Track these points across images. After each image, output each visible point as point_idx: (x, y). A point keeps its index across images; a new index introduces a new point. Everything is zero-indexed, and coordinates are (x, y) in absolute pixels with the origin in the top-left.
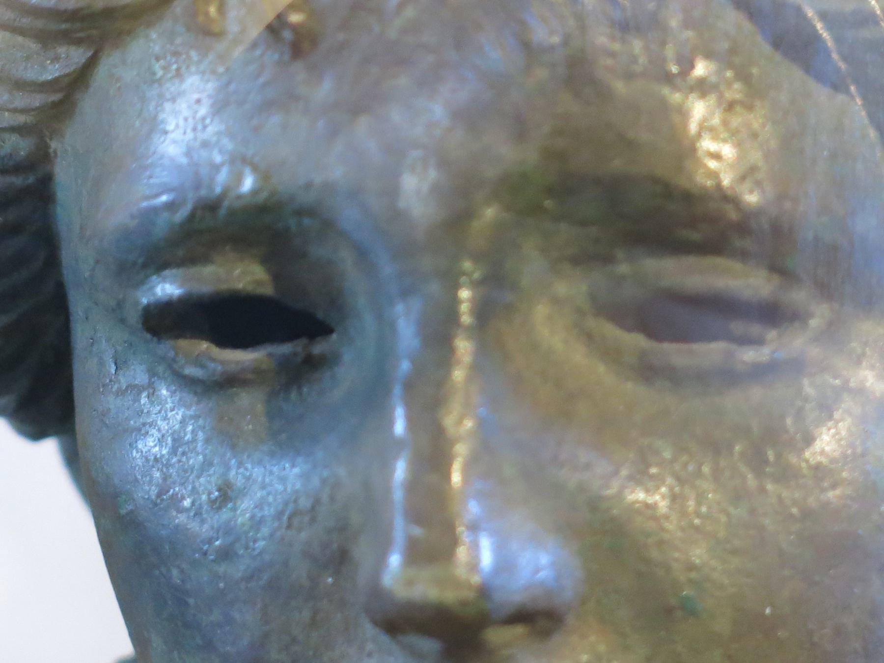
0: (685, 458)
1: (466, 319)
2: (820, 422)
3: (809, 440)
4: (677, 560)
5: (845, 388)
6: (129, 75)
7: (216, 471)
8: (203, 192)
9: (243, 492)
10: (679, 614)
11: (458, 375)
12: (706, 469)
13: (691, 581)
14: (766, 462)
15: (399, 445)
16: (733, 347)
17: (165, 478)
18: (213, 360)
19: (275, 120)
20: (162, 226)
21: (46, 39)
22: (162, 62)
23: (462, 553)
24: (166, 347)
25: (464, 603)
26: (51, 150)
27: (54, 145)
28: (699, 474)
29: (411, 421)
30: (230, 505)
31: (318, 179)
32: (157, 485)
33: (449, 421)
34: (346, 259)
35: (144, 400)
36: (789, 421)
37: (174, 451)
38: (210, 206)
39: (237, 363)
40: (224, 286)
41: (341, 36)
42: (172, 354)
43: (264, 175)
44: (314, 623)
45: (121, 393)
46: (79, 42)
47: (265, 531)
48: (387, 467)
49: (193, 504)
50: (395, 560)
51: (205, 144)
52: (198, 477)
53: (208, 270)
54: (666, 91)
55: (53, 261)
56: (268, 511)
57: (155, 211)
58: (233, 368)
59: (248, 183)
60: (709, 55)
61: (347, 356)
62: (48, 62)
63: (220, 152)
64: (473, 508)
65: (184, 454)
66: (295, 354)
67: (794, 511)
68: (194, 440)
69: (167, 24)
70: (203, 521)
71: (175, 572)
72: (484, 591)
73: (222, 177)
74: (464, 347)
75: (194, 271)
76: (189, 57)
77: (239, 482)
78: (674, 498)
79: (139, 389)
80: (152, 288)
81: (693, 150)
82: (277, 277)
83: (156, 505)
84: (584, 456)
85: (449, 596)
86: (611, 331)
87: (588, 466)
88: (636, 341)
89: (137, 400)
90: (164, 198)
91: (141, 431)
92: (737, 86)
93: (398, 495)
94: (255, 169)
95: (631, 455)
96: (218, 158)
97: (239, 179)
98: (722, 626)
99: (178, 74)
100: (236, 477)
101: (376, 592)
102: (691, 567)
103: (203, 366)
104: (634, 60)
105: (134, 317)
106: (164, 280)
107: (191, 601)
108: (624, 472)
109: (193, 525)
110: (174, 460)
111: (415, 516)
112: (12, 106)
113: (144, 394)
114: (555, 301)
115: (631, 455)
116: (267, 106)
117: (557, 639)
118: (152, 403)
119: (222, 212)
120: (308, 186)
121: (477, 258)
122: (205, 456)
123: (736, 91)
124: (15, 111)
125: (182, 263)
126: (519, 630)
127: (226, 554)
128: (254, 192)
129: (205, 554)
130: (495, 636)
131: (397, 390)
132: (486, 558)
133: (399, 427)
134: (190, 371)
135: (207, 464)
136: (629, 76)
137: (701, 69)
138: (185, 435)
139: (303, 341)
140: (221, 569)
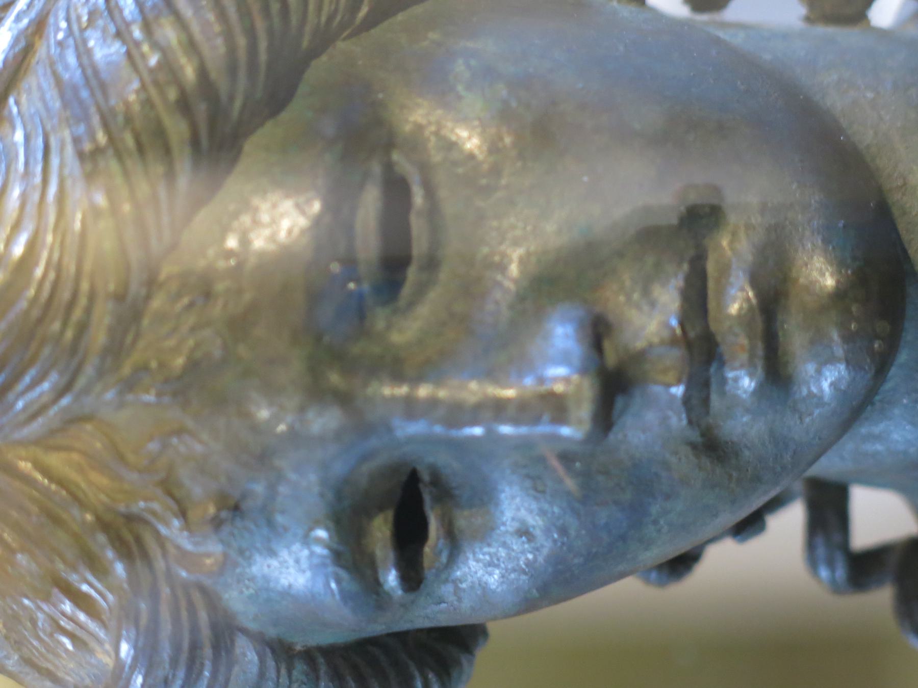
2: (461, 151)
3: (471, 156)
5: (437, 133)
7: (509, 540)
8: (328, 561)
9: (523, 522)
11: (442, 394)
12: (495, 223)
15: (490, 432)
17: (514, 570)
18: (436, 545)
19: (280, 519)
20: (352, 586)
22: (244, 589)
23: (559, 388)
24: (429, 574)
26: (302, 649)
27: (298, 648)
29: (474, 423)
30: (531, 530)
32: (519, 576)
34: (367, 468)
35: (464, 586)
37: (497, 566)
38: (337, 557)
39: (438, 530)
42: (434, 571)
43: (317, 524)
45: (460, 600)
47: (546, 506)
49: (530, 552)
50: (566, 431)
51: (297, 561)
52: (513, 550)
55: (373, 641)
57: (341, 591)
59: (322, 533)
60: (223, 239)
61: (430, 459)
62: (246, 659)
63: (301, 551)
64: (529, 381)
65: (498, 560)
68: (489, 554)
70: (542, 546)
71: (576, 561)
73: (319, 550)
75: (379, 562)
77: (516, 525)
78: (516, 243)
79: (457, 588)
80: (392, 589)
82: (381, 509)
83: (532, 576)
84: (490, 307)
86: (407, 291)
87: (497, 303)
88: (412, 274)
89: (464, 590)
90: (333, 585)
91: (484, 587)
93: (523, 430)
94: (311, 529)
96: (306, 552)
97: (318, 541)
100: (511, 526)
103: (440, 552)
105: (411, 596)
106: (386, 581)
107: (594, 550)
109: (545, 551)
110: (502, 565)
112: (276, 679)
113: (460, 585)
114: (389, 327)
116: (270, 523)
118: (466, 581)
119: (341, 548)
120: (322, 495)
122: (499, 546)
123: (246, 219)
124: (278, 677)
126: (607, 345)
127: (563, 531)
128: (327, 529)
129: (563, 544)
130: (611, 359)
131: (455, 433)
132: (560, 371)
133: (478, 431)
134: (444, 558)
135: (504, 545)
138: (485, 559)
139: (421, 486)
140: (572, 533)
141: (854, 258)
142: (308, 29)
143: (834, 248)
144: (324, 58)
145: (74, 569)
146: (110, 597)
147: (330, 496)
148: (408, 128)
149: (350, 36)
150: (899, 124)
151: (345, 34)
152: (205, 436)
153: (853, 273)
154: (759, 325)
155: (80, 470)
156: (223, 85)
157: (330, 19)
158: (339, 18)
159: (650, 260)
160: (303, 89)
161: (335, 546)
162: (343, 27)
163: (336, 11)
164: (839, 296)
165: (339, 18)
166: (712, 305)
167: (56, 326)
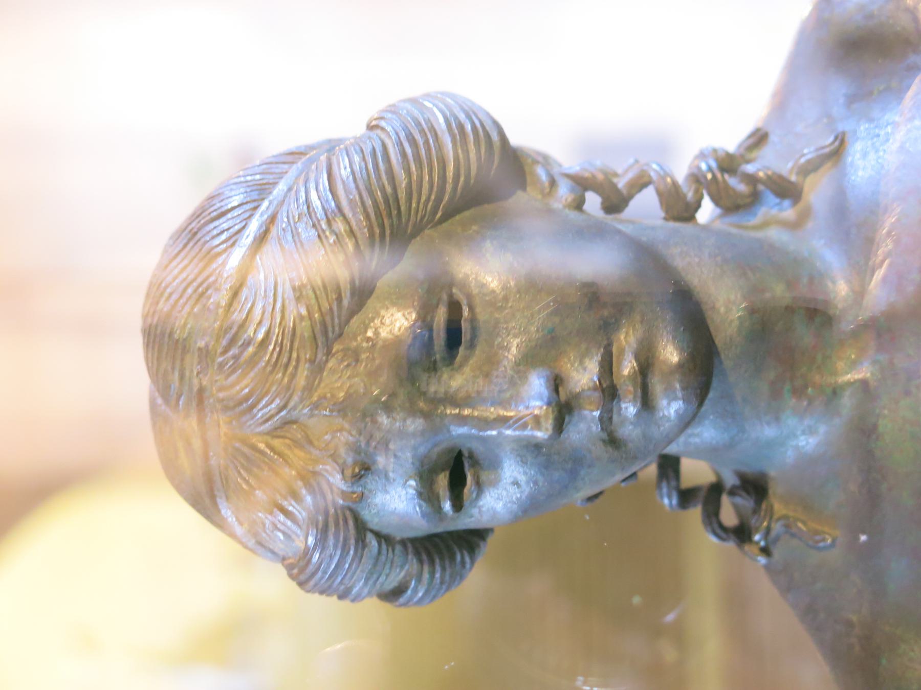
0: (501, 333)
1: (457, 411)
4: (536, 336)
6: (376, 520)
9: (515, 478)
10: (553, 334)
13: (542, 331)
14: (502, 306)
15: (500, 434)
16: (463, 319)
21: (364, 546)
24: (466, 503)
25: (553, 412)
28: (506, 328)
29: (492, 429)
31: (410, 460)
33: (492, 417)
36: (487, 298)
40: (447, 488)
41: (363, 454)
43: (410, 477)
44: (559, 454)
45: (481, 516)
46: (365, 536)
48: (507, 436)
53: (441, 493)
54: (378, 346)
56: (521, 470)
57: (422, 512)
58: (473, 482)
61: (469, 445)
66: (468, 462)
67: (518, 296)
69: (359, 509)
72: (549, 404)
74: (466, 412)
76: (370, 502)
78: (515, 336)
80: (448, 511)
81: (397, 337)
82: (443, 470)
85: (551, 416)
88: (462, 350)
92: (376, 321)
94: (407, 481)
95: (501, 352)
97: (410, 486)
98: (557, 320)
99: (376, 505)
100: (510, 480)
101: (550, 438)
102: (538, 330)
103: (473, 493)
104: (367, 357)
105: (457, 515)
108: (506, 354)
111: (524, 426)
115: (501, 352)
117: (563, 375)
120: (413, 463)
121: (436, 409)
125: (439, 502)
126: (560, 389)
127: (536, 483)
130: (563, 397)
133: (494, 433)
134: (474, 495)
136: (374, 359)
137: (370, 334)
140: (541, 484)
145: (286, 499)
150: (712, 275)
151: (429, 226)
154: (639, 379)
157: (423, 217)
158: (426, 218)
162: (429, 222)
164: (680, 365)
165: (426, 218)
166: (614, 369)
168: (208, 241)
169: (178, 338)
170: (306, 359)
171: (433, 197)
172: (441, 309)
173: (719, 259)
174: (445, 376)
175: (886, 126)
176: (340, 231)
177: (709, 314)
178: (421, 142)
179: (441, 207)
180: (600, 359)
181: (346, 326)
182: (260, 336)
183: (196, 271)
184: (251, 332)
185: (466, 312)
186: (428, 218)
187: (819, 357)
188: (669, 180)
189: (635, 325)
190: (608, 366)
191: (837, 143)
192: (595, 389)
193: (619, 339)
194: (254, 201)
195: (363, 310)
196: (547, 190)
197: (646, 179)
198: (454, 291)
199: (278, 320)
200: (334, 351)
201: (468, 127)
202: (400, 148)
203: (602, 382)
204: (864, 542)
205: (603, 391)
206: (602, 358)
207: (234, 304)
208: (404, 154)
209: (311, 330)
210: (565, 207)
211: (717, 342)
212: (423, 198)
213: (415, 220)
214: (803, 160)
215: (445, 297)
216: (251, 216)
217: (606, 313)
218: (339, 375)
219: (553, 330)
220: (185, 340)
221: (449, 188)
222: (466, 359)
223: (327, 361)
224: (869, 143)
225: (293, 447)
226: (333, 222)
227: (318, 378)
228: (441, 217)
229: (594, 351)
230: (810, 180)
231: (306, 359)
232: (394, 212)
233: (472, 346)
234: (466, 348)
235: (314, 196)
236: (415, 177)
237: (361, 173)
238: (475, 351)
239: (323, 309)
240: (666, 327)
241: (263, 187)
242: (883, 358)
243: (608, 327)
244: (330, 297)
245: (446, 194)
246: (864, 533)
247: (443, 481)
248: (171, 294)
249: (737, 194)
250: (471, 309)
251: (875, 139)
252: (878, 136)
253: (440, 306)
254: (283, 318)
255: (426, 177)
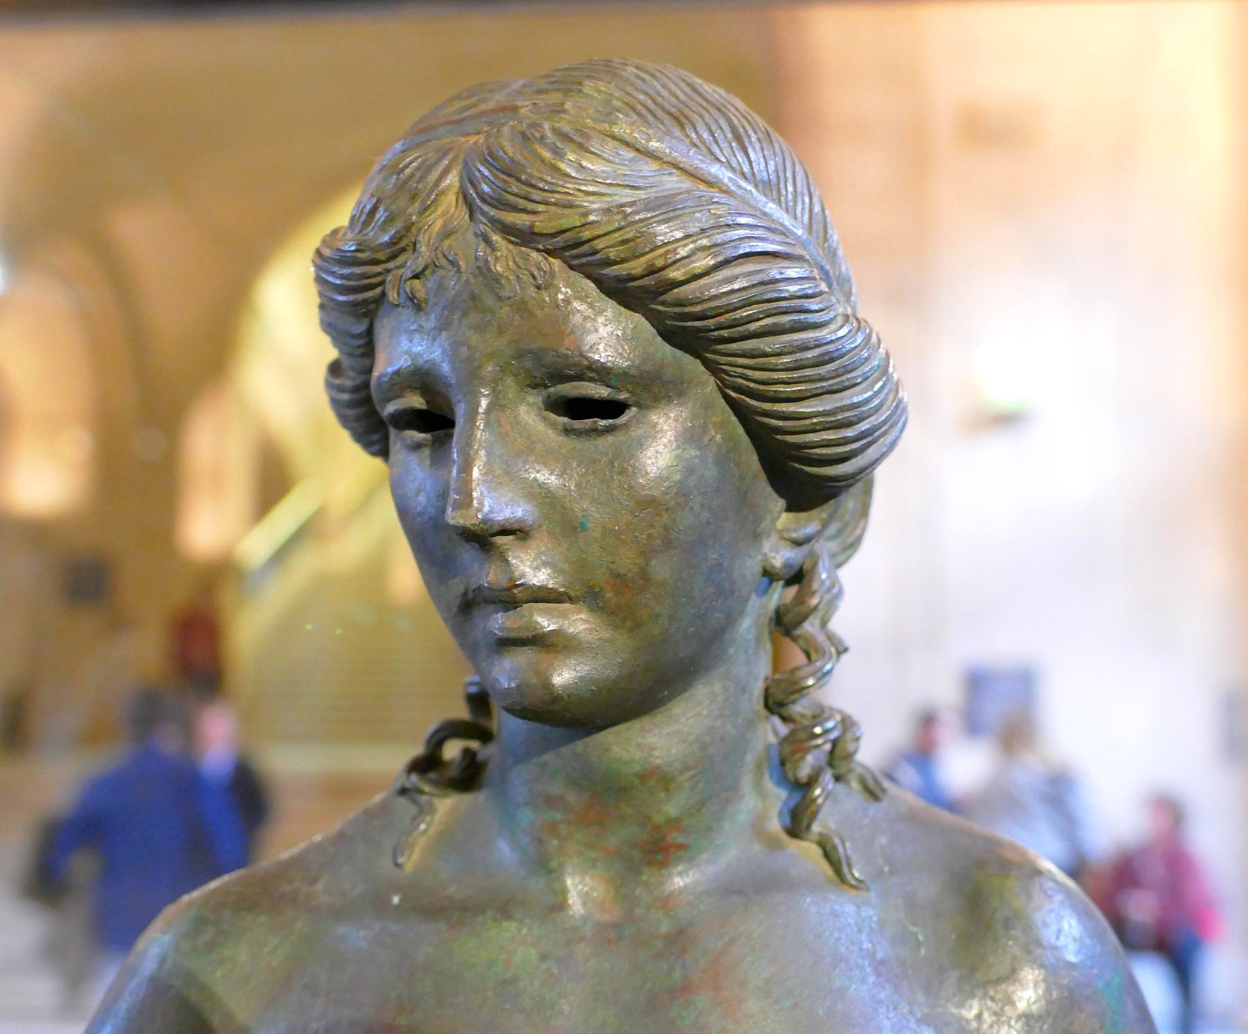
78: (578, 485)
82: (428, 403)
86: (553, 416)
114: (529, 404)
117: (529, 542)
141: (569, 696)
142: (717, 357)
143: (577, 683)
144: (703, 368)
145: (385, 211)
146: (372, 233)
147: (426, 367)
148: (654, 418)
149: (717, 385)
150: (685, 729)
151: (718, 382)
152: (457, 287)
153: (559, 694)
154: (525, 635)
155: (444, 214)
156: (669, 297)
157: (725, 372)
158: (727, 377)
159: (566, 567)
160: (679, 353)
161: (402, 371)
162: (722, 380)
163: (732, 376)
164: (548, 685)
165: (727, 377)
166: (541, 605)
167: (514, 189)
168: (703, 120)
169: (584, 84)
170: (535, 222)
171: (752, 385)
172: (606, 390)
173: (708, 739)
174: (531, 399)
175: (871, 942)
176: (693, 262)
177: (645, 721)
178: (822, 370)
179: (743, 397)
180: (550, 586)
181: (583, 274)
182: (563, 166)
183: (666, 105)
184: (571, 157)
185: (603, 423)
186: (727, 380)
187: (594, 854)
188: (810, 682)
189: (597, 631)
190: (543, 596)
191: (853, 882)
192: (512, 579)
193: (579, 612)
194: (753, 174)
195: (603, 296)
196: (786, 536)
197: (814, 656)
198: (634, 409)
199: (584, 188)
200: (551, 259)
201: (850, 433)
202: (812, 343)
203: (520, 589)
204: (391, 900)
205: (509, 589)
206: (551, 588)
207: (614, 142)
208: (806, 348)
209: (569, 227)
210: (765, 555)
211: (603, 733)
212: (749, 373)
213: (722, 362)
214: (837, 841)
215: (622, 396)
216: (734, 170)
217: (609, 595)
218: (522, 267)
219: (584, 529)
220: (580, 91)
221: (767, 406)
222: (553, 425)
223: (538, 250)
224: (852, 921)
225: (445, 218)
226: (707, 253)
227: (517, 241)
228: (732, 397)
229: (560, 579)
230: (816, 851)
231: (535, 222)
232: (725, 333)
233: (567, 431)
234: (564, 425)
235: (742, 232)
236: (773, 360)
237: (773, 291)
238: (562, 436)
239: (596, 242)
240: (596, 669)
241: (774, 188)
242: (588, 931)
243: (590, 597)
244: (611, 249)
245: (759, 403)
246: (402, 900)
247: (416, 401)
248: (643, 80)
249: (797, 763)
250: (609, 430)
251: (855, 929)
252: (860, 931)
253: (609, 390)
254: (588, 193)
255: (775, 375)
